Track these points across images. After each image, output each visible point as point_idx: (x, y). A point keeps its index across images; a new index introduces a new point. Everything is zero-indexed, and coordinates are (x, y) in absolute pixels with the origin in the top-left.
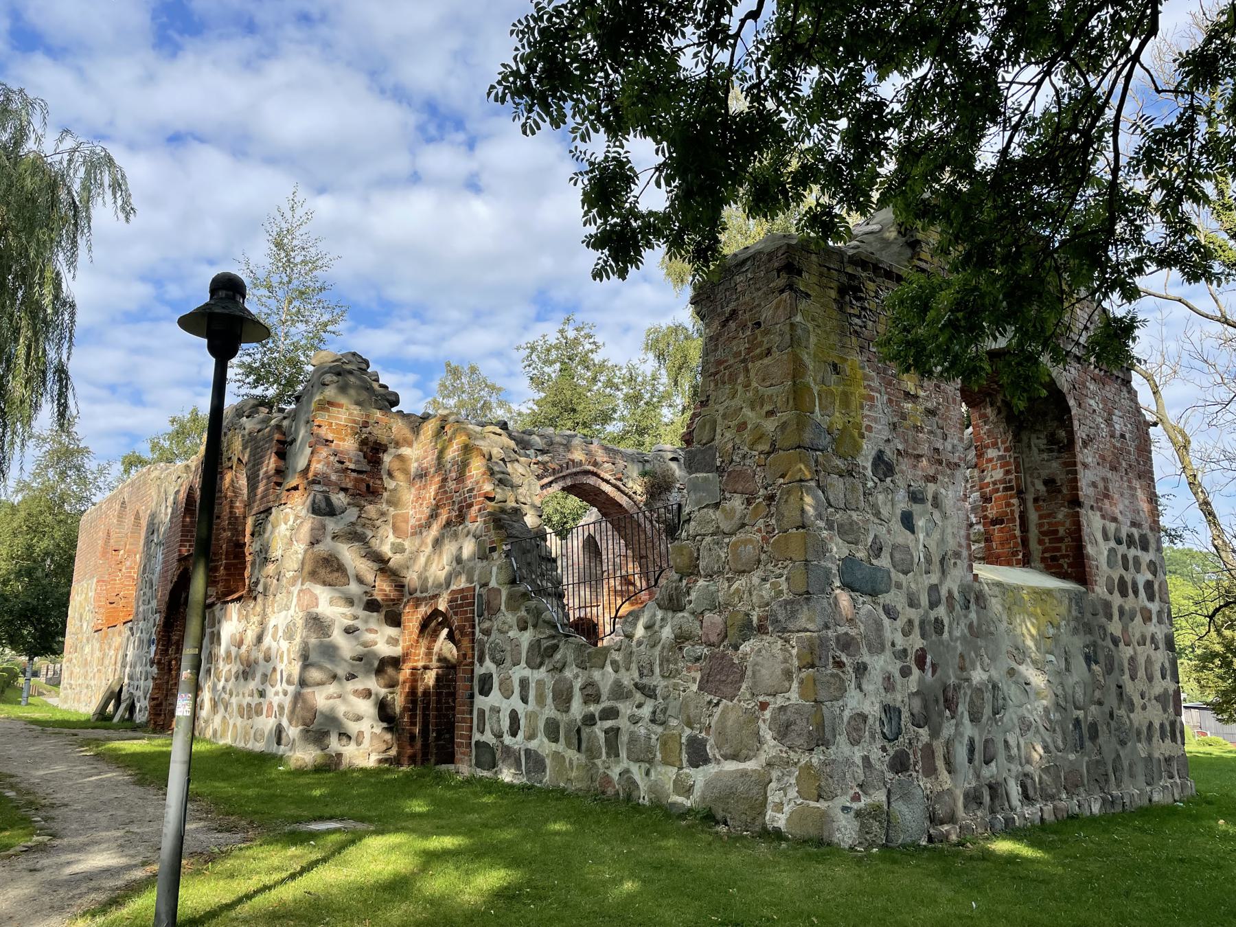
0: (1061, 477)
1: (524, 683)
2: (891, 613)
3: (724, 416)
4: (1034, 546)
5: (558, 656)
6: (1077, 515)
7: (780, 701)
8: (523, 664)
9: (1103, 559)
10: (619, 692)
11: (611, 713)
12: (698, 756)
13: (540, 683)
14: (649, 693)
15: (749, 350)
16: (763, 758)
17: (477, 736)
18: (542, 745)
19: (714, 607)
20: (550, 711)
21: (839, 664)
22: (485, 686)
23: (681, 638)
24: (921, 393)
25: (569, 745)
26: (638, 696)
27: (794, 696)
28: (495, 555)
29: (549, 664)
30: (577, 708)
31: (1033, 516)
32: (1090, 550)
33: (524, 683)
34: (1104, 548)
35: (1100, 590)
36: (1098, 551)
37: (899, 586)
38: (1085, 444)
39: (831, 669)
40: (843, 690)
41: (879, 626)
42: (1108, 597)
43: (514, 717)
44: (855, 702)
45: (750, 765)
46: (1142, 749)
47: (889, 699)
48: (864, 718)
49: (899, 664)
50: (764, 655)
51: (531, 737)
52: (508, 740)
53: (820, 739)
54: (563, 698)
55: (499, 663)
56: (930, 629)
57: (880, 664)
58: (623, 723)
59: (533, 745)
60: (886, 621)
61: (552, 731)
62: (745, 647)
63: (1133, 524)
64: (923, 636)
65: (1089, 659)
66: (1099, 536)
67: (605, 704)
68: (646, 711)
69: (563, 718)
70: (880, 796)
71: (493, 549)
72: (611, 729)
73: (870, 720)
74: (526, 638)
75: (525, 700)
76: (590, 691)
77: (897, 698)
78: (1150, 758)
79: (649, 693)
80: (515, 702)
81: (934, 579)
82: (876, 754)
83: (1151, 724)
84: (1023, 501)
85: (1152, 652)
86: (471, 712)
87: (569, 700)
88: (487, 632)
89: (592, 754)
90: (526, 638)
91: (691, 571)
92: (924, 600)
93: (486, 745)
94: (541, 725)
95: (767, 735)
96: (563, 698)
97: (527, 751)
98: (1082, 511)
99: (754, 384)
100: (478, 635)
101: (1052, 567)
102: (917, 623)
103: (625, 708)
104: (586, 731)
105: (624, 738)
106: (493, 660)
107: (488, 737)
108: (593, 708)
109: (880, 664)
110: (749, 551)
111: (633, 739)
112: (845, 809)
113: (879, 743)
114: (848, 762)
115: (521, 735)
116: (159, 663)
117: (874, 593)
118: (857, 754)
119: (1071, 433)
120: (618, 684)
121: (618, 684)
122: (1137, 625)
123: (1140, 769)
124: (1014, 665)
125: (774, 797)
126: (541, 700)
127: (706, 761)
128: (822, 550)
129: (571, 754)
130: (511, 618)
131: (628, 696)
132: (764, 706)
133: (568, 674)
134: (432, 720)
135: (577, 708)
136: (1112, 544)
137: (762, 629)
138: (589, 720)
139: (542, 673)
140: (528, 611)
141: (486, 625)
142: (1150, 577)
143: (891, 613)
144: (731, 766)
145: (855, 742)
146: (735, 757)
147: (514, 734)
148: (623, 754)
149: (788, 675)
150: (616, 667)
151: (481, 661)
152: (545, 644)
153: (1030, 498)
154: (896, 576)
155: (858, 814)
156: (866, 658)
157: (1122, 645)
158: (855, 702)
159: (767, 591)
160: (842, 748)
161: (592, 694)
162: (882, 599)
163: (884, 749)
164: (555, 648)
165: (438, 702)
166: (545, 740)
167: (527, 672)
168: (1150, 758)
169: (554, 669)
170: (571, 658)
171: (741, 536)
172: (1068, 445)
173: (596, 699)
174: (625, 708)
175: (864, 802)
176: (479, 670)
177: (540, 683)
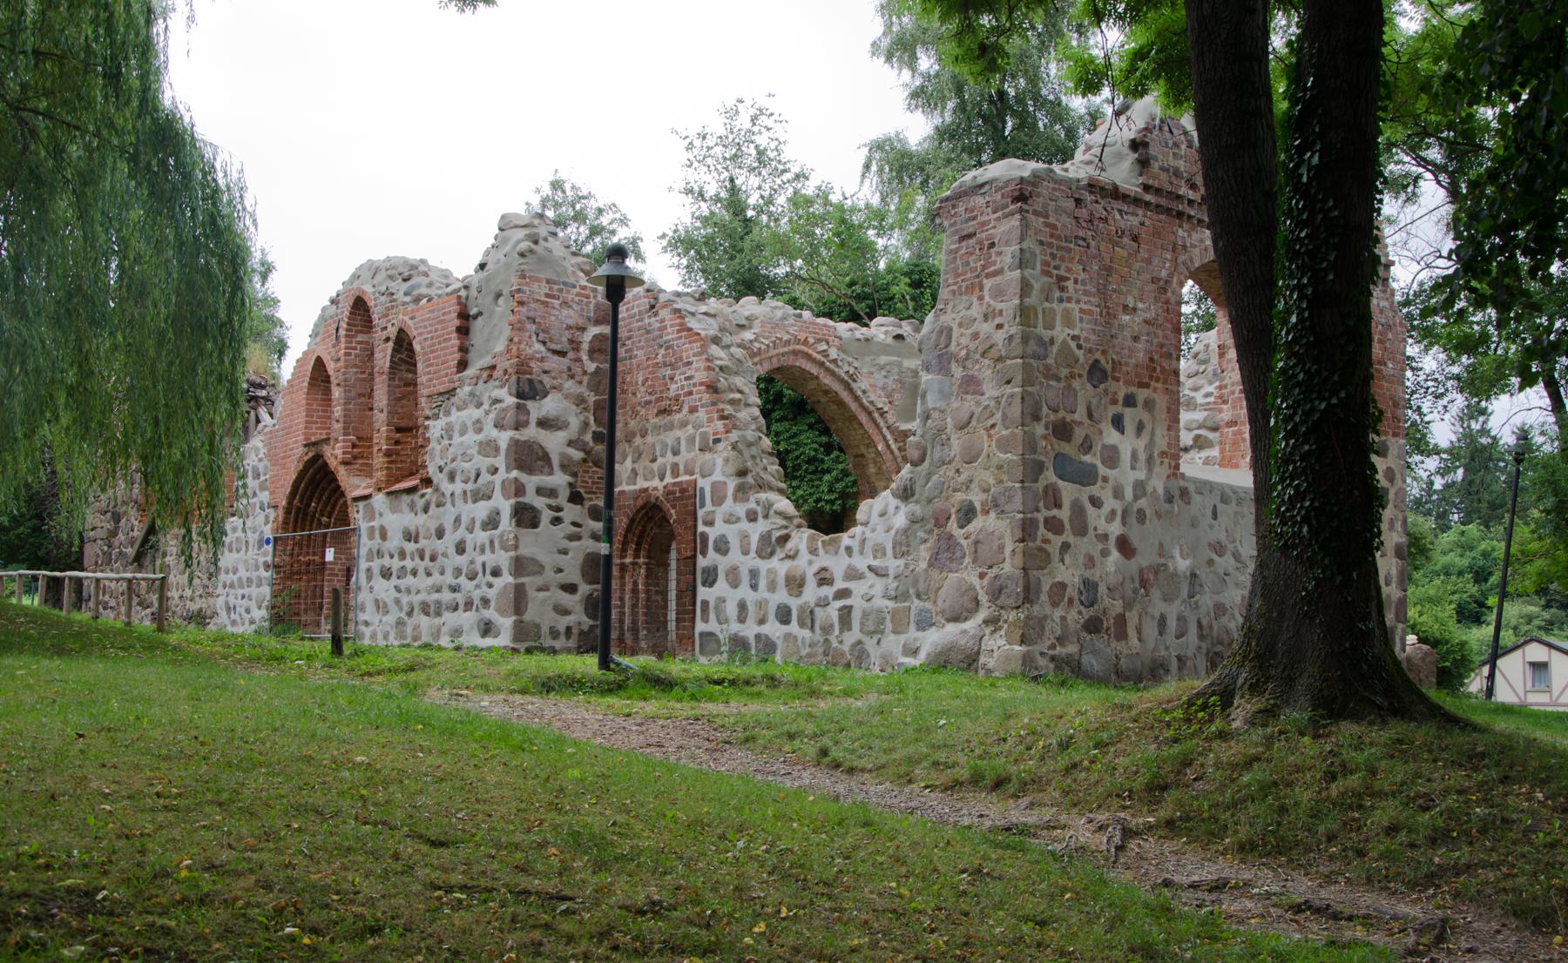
1: (754, 574)
3: (960, 325)
5: (789, 545)
7: (995, 570)
8: (753, 554)
11: (843, 594)
15: (984, 267)
17: (700, 626)
18: (773, 629)
22: (710, 578)
24: (1140, 305)
25: (802, 625)
28: (720, 446)
33: (754, 574)
37: (1105, 480)
43: (742, 606)
47: (1088, 574)
49: (1100, 546)
51: (762, 622)
56: (1133, 519)
59: (766, 629)
61: (784, 615)
64: (1124, 523)
67: (840, 584)
69: (794, 603)
70: (1072, 649)
71: (717, 441)
72: (845, 607)
73: (1069, 590)
75: (754, 587)
76: (823, 575)
77: (1094, 574)
81: (1141, 475)
86: (694, 604)
89: (827, 629)
92: (1129, 493)
93: (711, 634)
96: (795, 584)
99: (987, 298)
102: (1119, 513)
103: (858, 588)
104: (819, 612)
106: (717, 550)
107: (712, 626)
112: (1042, 654)
116: (276, 567)
124: (1215, 557)
126: (772, 587)
131: (859, 576)
134: (641, 618)
135: (811, 593)
140: (758, 503)
144: (952, 628)
147: (742, 620)
151: (704, 554)
152: (776, 534)
154: (1102, 470)
155: (1053, 659)
156: (1071, 539)
161: (824, 579)
163: (1080, 613)
165: (648, 599)
166: (777, 624)
169: (788, 557)
174: (858, 588)
176: (702, 562)
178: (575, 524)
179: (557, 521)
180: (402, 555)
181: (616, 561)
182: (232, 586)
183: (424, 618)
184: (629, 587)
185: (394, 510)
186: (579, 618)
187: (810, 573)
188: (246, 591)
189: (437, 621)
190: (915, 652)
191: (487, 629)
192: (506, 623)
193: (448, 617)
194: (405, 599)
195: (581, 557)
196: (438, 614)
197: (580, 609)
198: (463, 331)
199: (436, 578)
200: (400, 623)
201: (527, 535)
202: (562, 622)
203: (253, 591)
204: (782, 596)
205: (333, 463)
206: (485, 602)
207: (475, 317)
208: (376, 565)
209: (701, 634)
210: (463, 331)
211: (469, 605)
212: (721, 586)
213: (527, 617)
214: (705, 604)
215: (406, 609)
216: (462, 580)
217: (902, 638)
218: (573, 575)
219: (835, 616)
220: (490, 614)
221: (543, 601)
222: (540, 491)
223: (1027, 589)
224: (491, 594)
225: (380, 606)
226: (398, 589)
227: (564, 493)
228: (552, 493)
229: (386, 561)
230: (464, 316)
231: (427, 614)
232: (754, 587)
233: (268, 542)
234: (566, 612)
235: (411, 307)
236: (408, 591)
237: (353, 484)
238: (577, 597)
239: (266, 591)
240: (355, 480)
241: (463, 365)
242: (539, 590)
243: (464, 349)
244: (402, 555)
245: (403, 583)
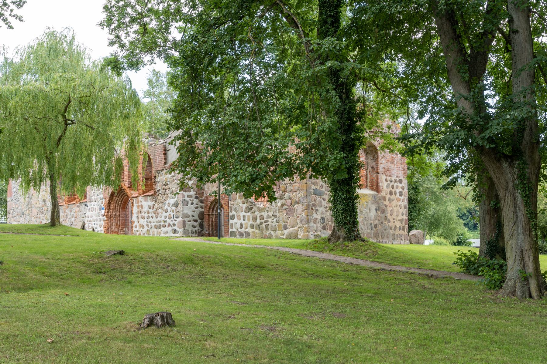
0: (375, 166)
1: (244, 216)
2: (324, 199)
4: (369, 184)
5: (253, 210)
6: (378, 176)
9: (385, 187)
10: (269, 217)
11: (267, 221)
12: (285, 228)
13: (248, 216)
14: (275, 216)
16: (298, 227)
17: (230, 230)
19: (289, 198)
20: (251, 222)
21: (312, 209)
22: (233, 218)
23: (282, 205)
25: (256, 229)
26: (273, 217)
27: (304, 215)
29: (251, 211)
30: (258, 221)
31: (369, 176)
32: (380, 184)
33: (244, 216)
34: (386, 184)
35: (383, 194)
36: (383, 184)
38: (382, 158)
39: (310, 210)
40: (313, 214)
41: (321, 202)
42: (385, 196)
43: (241, 225)
44: (315, 216)
45: (295, 228)
46: (392, 232)
47: (322, 216)
48: (317, 219)
50: (299, 208)
51: (247, 228)
52: (240, 230)
53: (308, 222)
54: (255, 219)
55: (237, 212)
57: (321, 209)
58: (269, 223)
59: (247, 230)
60: (323, 201)
61: (252, 227)
62: (295, 206)
63: (397, 177)
65: (376, 210)
66: (384, 181)
67: (265, 219)
68: (275, 220)
69: (255, 224)
74: (244, 206)
75: (244, 220)
77: (324, 216)
78: (394, 234)
79: (275, 216)
80: (242, 221)
82: (319, 225)
83: (396, 226)
84: (367, 172)
85: (399, 209)
87: (256, 219)
88: (233, 205)
89: (262, 230)
90: (244, 206)
91: (285, 191)
93: (233, 232)
94: (249, 225)
95: (299, 222)
96: (255, 219)
97: (245, 232)
98: (379, 175)
100: (230, 205)
101: (372, 188)
103: (270, 220)
104: (261, 226)
105: (270, 226)
106: (235, 211)
107: (234, 230)
108: (262, 221)
109: (321, 209)
110: (296, 188)
111: (272, 226)
113: (320, 223)
114: (313, 227)
115: (243, 228)
117: (320, 196)
118: (315, 225)
119: (378, 156)
120: (268, 215)
121: (268, 215)
122: (394, 203)
123: (390, 237)
125: (299, 233)
126: (249, 220)
127: (287, 228)
128: (310, 187)
129: (257, 231)
130: (240, 201)
132: (298, 217)
133: (256, 213)
135: (258, 221)
136: (389, 182)
137: (298, 203)
138: (261, 223)
139: (249, 214)
141: (232, 203)
142: (401, 190)
143: (324, 199)
144: (292, 229)
145: (314, 223)
146: (292, 227)
147: (241, 228)
148: (270, 229)
149: (303, 211)
150: (268, 211)
151: (231, 212)
152: (250, 207)
153: (368, 171)
156: (318, 208)
157: (388, 207)
158: (315, 216)
159: (299, 196)
160: (312, 224)
162: (322, 197)
164: (252, 208)
167: (245, 214)
168: (394, 234)
170: (256, 210)
171: (295, 184)
172: (377, 159)
173: (263, 219)
174: (270, 220)
175: (315, 234)
176: (230, 214)
177: (248, 216)
178: (197, 204)
179: (192, 204)
180: (148, 213)
181: (408, 282)
182: (90, 221)
183: (155, 230)
184: (211, 220)
185: (145, 201)
186: (198, 228)
187: (258, 216)
188: (96, 223)
189: (160, 230)
190: (284, 235)
191: (175, 231)
192: (180, 230)
193: (163, 229)
194: (149, 224)
195: (198, 213)
196: (160, 228)
197: (198, 226)
198: (165, 154)
199: (159, 219)
200: (148, 231)
201: (185, 207)
202: (194, 229)
203: (98, 222)
204: (251, 222)
205: (125, 187)
206: (174, 225)
207: (168, 151)
208: (140, 215)
209: (231, 232)
210: (165, 154)
211: (169, 225)
212: (236, 220)
213: (186, 228)
214: (232, 224)
215: (150, 227)
216: (167, 219)
217: (432, 172)
218: (196, 217)
219: (264, 226)
220: (176, 228)
221: (189, 225)
222: (188, 196)
223: (308, 220)
224: (176, 223)
225: (142, 226)
226: (147, 221)
227: (194, 196)
228: (191, 197)
229: (143, 214)
230: (165, 150)
231: (157, 228)
232: (244, 220)
233: (103, 209)
234: (195, 227)
235: (149, 147)
236: (150, 222)
237: (133, 194)
238: (198, 223)
239: (102, 223)
240: (132, 192)
241: (165, 163)
242: (188, 221)
243: (165, 159)
244: (148, 213)
245: (149, 220)
